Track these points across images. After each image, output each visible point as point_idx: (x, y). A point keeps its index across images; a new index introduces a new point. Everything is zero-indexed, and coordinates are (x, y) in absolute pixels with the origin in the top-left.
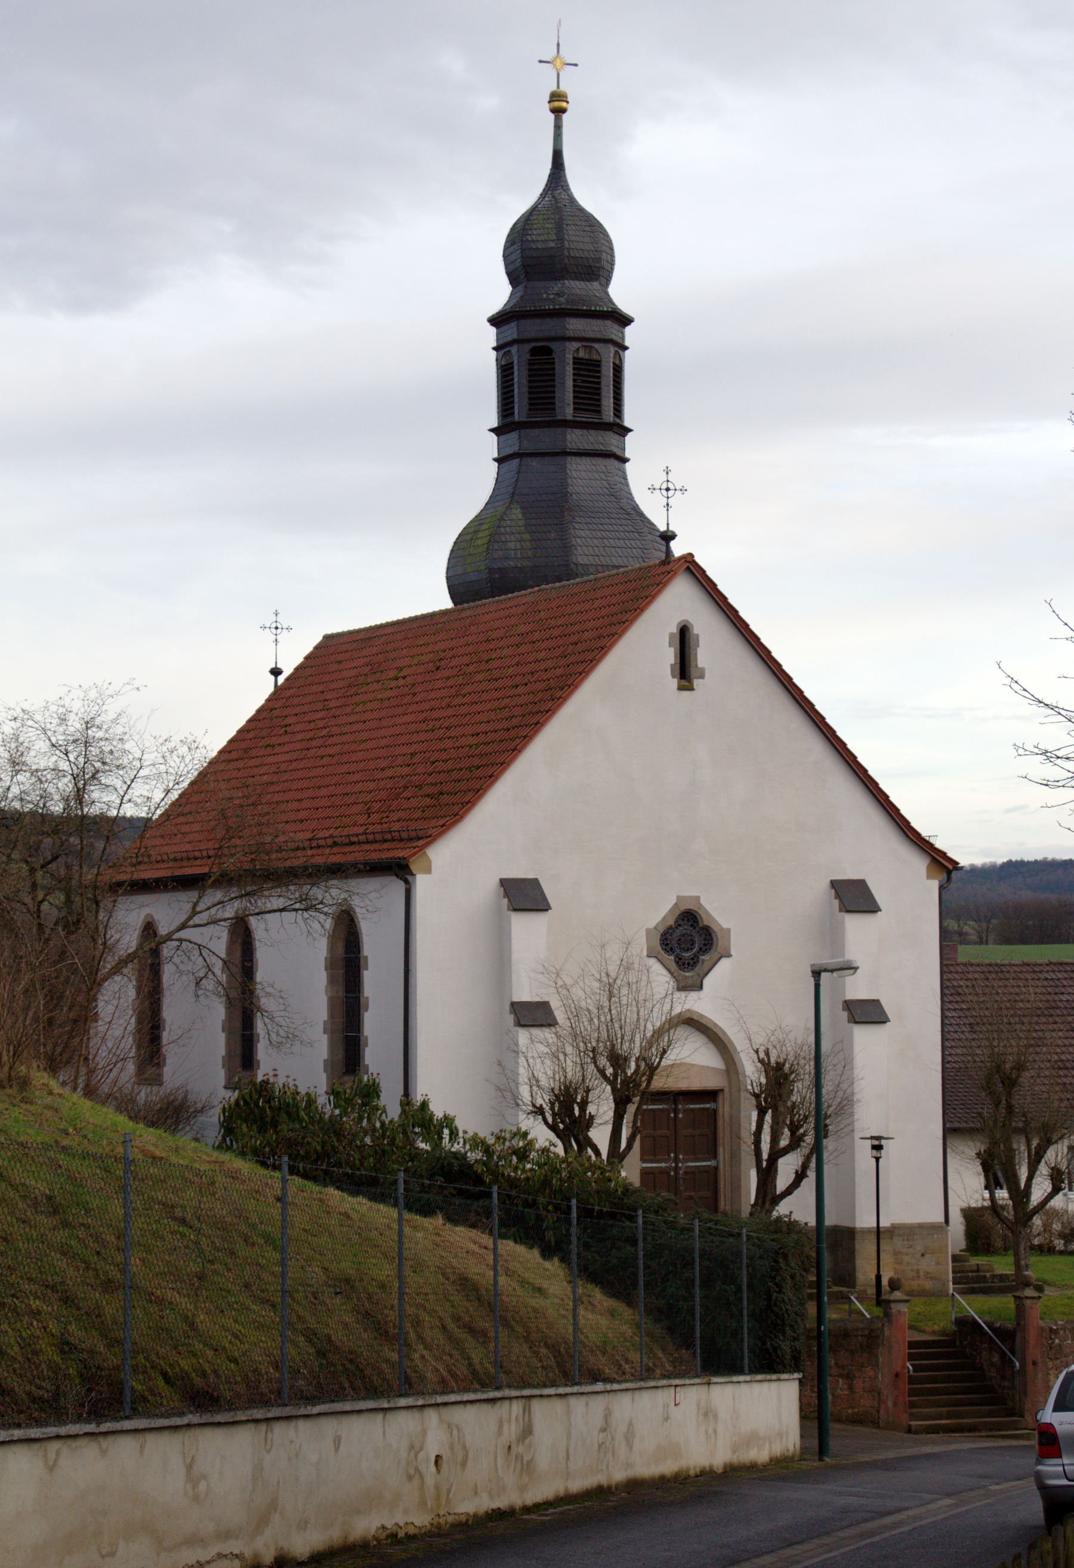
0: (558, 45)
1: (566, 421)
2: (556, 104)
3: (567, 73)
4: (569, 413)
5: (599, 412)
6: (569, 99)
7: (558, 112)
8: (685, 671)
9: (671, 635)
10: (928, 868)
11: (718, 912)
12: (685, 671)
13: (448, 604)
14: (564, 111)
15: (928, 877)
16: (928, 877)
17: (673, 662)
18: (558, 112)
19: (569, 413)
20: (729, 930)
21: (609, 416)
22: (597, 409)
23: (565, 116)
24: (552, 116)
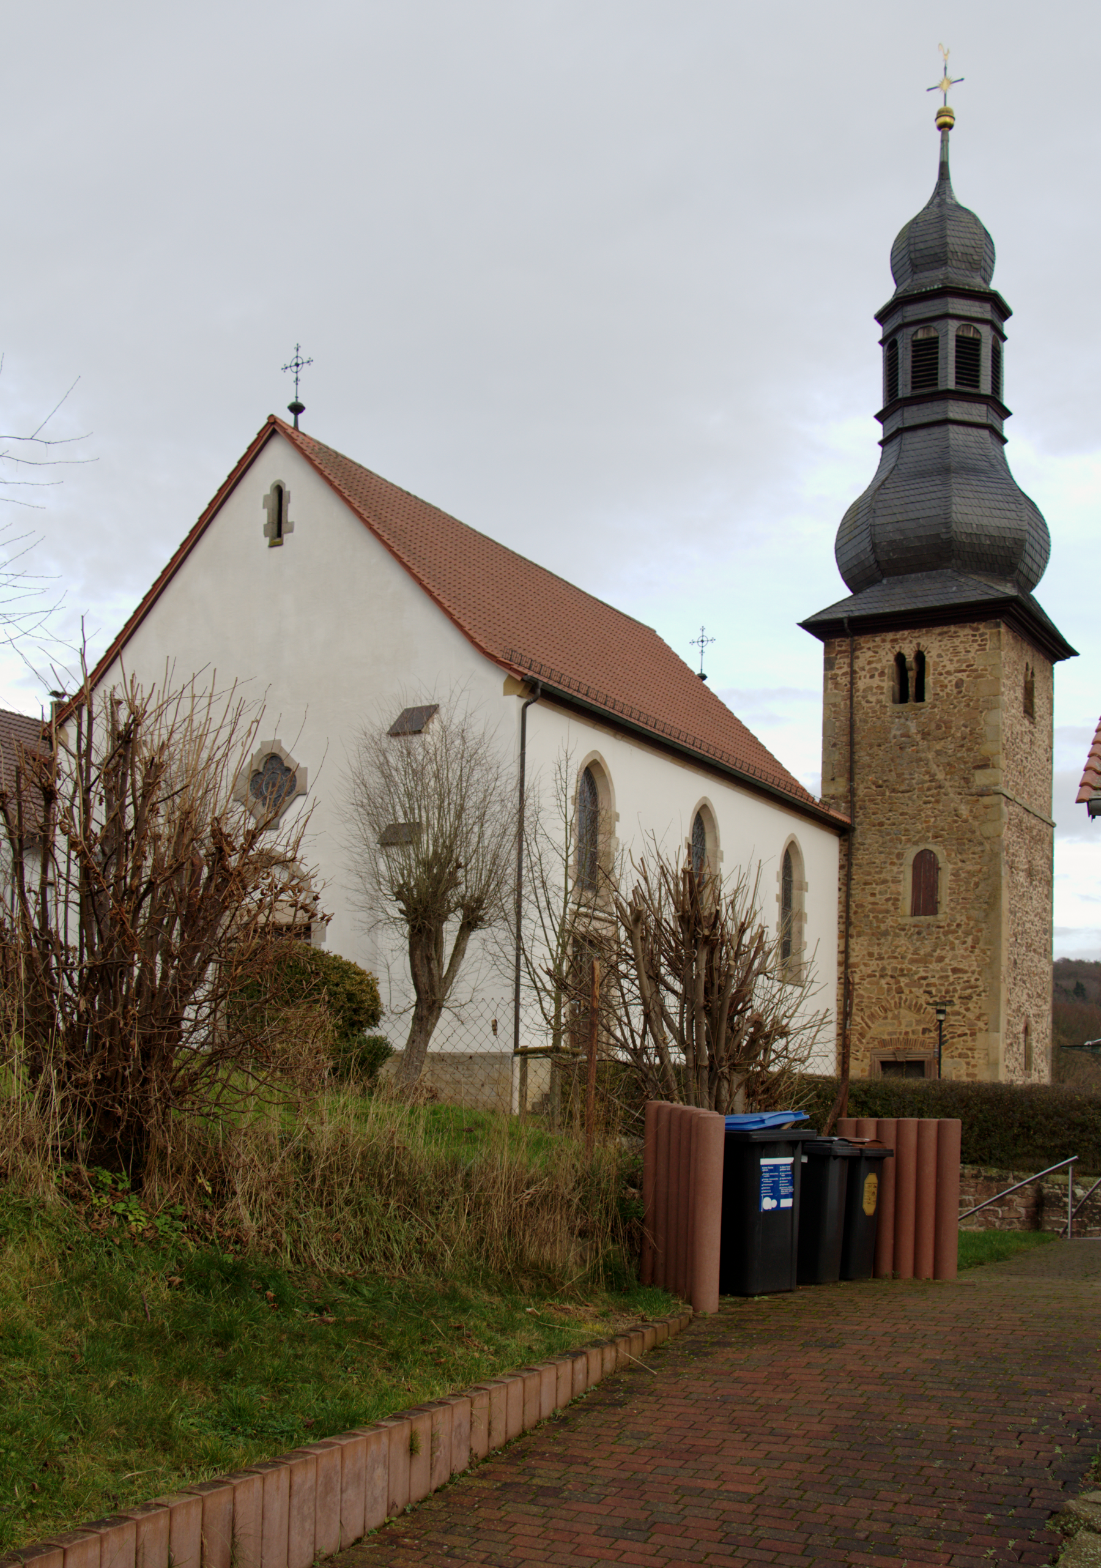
0: (945, 68)
1: (949, 391)
2: (942, 120)
3: (954, 91)
4: (951, 385)
5: (978, 387)
6: (955, 116)
7: (945, 127)
8: (278, 529)
9: (266, 497)
10: (506, 684)
11: (298, 756)
12: (278, 529)
13: (851, 594)
14: (951, 127)
15: (505, 694)
16: (505, 694)
17: (266, 522)
18: (945, 127)
19: (951, 385)
20: (306, 769)
21: (986, 388)
22: (975, 383)
23: (951, 133)
24: (939, 133)
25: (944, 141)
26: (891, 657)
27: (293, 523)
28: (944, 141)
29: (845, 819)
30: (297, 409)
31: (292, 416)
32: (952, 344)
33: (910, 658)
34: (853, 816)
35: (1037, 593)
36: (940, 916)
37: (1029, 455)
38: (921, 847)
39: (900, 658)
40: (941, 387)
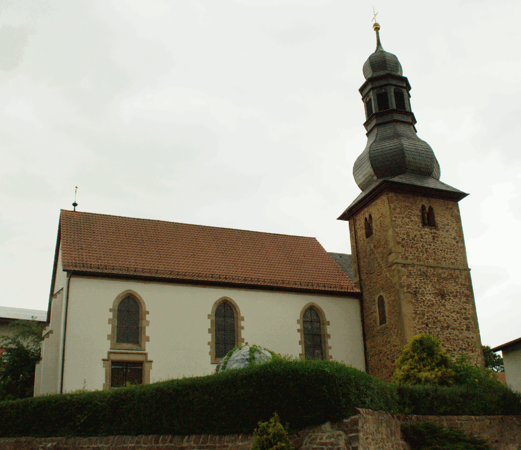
1: (394, 110)
18: (377, 28)
25: (378, 34)
26: (420, 206)
27: (109, 323)
28: (378, 34)
29: (358, 291)
30: (75, 205)
31: (73, 207)
32: (393, 94)
33: (367, 217)
34: (361, 288)
35: (441, 179)
36: (387, 323)
37: (425, 131)
38: (379, 295)
39: (423, 207)
40: (390, 108)
